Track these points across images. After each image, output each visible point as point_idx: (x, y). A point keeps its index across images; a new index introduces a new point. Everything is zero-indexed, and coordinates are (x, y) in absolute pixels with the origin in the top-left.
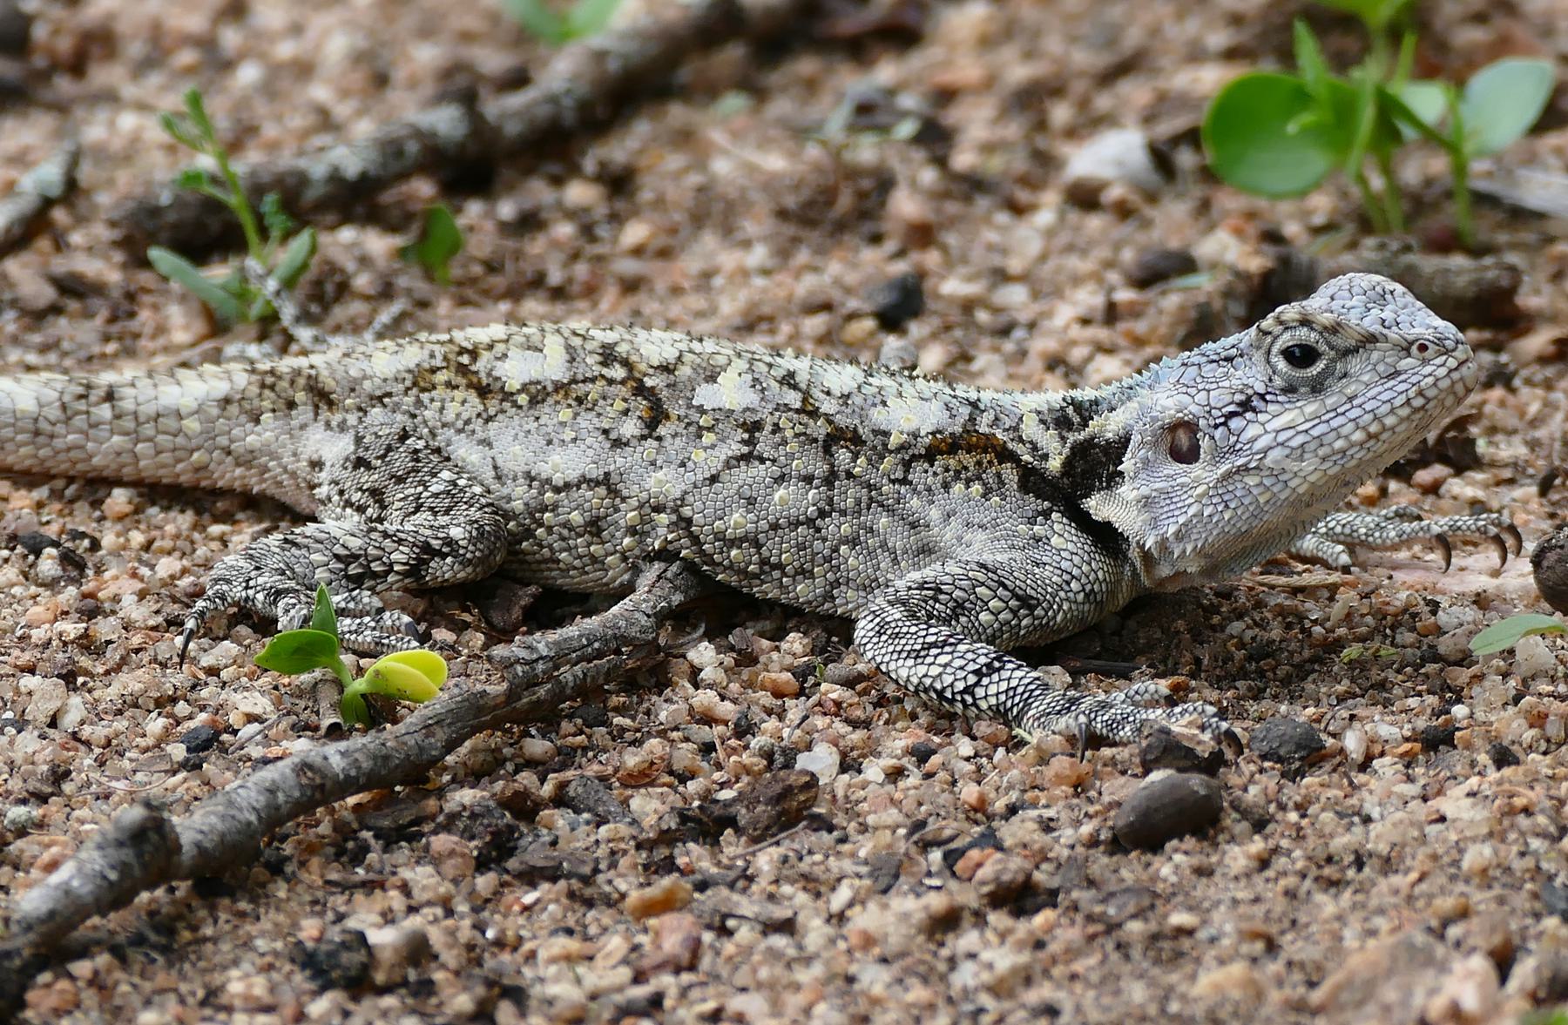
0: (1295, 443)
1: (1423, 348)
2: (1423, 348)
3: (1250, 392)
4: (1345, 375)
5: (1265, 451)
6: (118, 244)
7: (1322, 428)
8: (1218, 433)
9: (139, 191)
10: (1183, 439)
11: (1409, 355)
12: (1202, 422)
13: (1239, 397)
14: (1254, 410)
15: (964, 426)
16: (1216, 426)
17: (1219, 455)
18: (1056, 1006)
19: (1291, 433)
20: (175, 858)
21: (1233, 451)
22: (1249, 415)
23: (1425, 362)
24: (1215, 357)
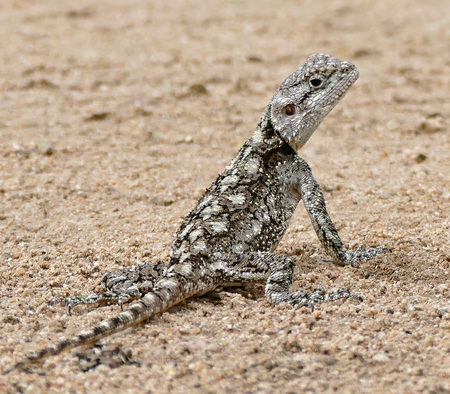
0: (321, 103)
1: (347, 70)
2: (347, 70)
3: (306, 93)
4: (330, 83)
5: (314, 107)
6: (94, 330)
7: (328, 97)
8: (300, 106)
9: (44, 348)
10: (290, 109)
11: (344, 73)
12: (295, 104)
13: (303, 95)
14: (308, 97)
15: (148, 204)
16: (299, 104)
17: (301, 111)
18: (425, 155)
19: (320, 100)
20: (55, 350)
21: (306, 109)
22: (307, 99)
23: (348, 73)
24: (291, 85)
